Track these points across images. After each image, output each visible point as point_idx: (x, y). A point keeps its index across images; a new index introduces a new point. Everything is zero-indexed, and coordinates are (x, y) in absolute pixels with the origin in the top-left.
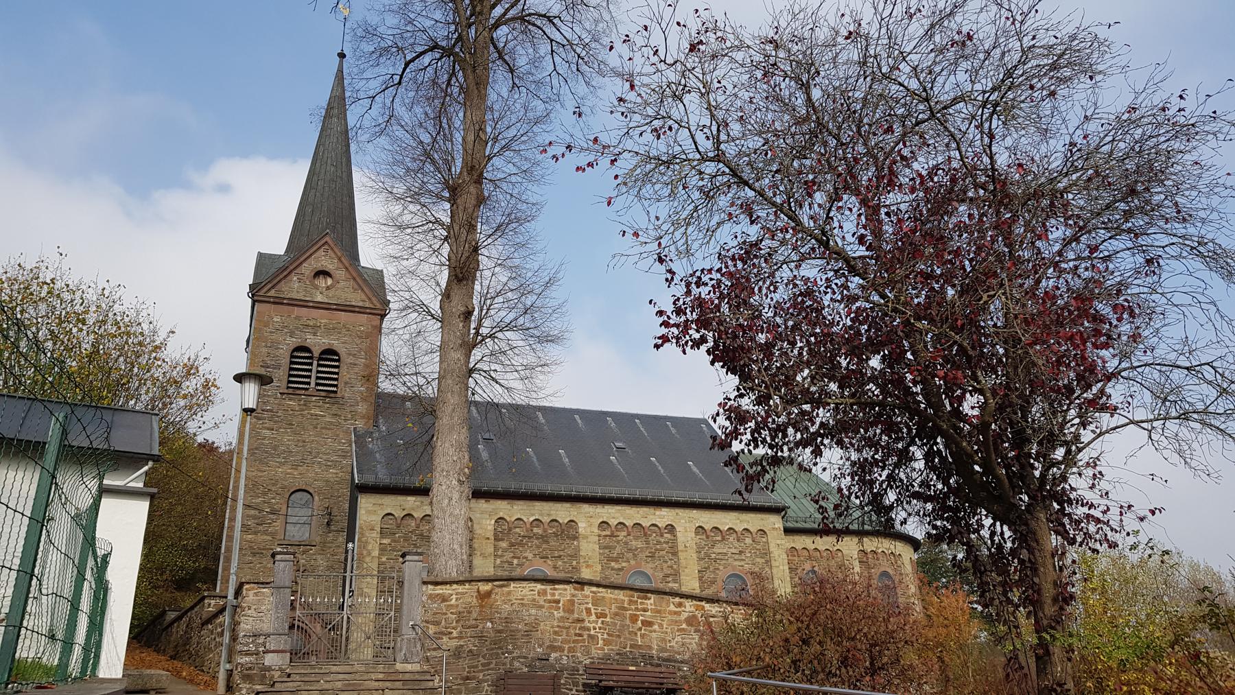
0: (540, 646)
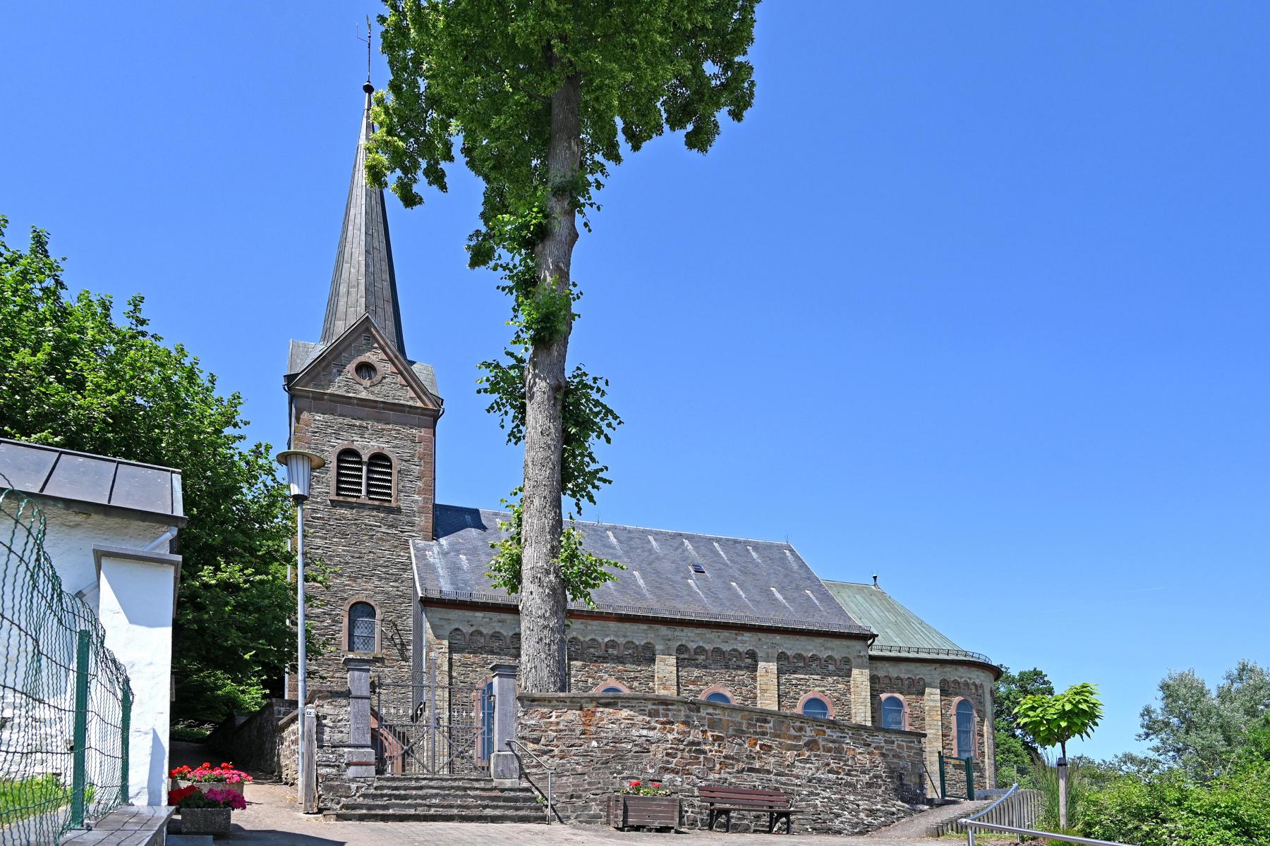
0: (652, 767)
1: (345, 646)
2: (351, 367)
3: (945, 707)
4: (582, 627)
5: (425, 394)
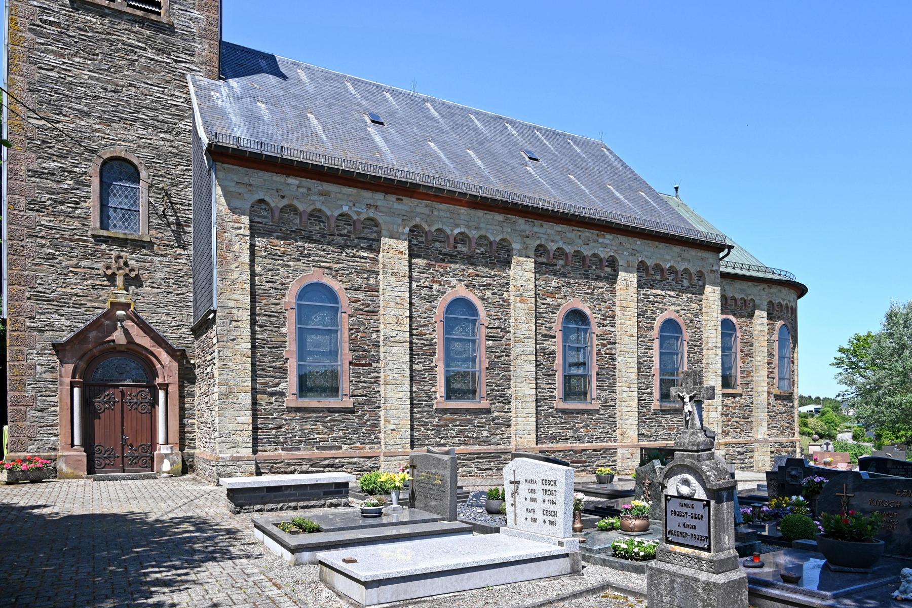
3: (771, 331)
4: (427, 211)
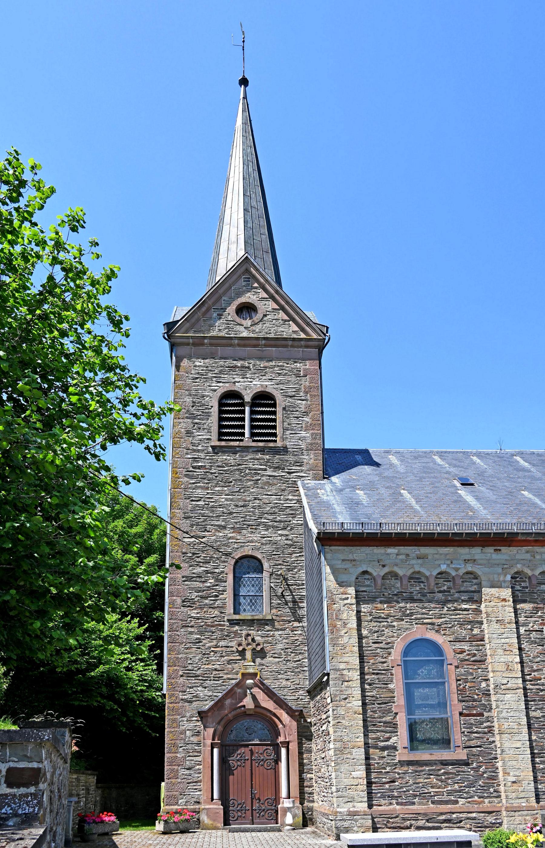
1: (230, 609)
2: (231, 309)
4: (528, 556)
5: (308, 324)
